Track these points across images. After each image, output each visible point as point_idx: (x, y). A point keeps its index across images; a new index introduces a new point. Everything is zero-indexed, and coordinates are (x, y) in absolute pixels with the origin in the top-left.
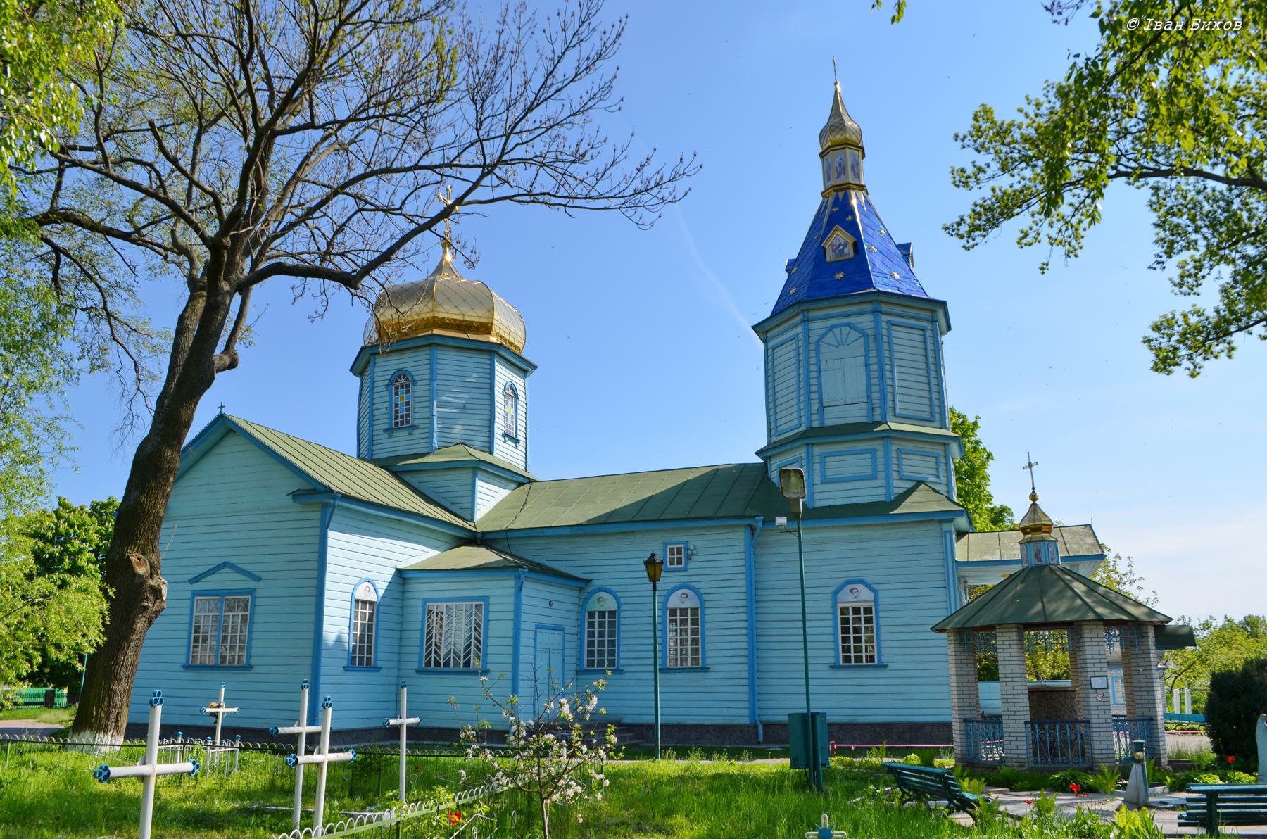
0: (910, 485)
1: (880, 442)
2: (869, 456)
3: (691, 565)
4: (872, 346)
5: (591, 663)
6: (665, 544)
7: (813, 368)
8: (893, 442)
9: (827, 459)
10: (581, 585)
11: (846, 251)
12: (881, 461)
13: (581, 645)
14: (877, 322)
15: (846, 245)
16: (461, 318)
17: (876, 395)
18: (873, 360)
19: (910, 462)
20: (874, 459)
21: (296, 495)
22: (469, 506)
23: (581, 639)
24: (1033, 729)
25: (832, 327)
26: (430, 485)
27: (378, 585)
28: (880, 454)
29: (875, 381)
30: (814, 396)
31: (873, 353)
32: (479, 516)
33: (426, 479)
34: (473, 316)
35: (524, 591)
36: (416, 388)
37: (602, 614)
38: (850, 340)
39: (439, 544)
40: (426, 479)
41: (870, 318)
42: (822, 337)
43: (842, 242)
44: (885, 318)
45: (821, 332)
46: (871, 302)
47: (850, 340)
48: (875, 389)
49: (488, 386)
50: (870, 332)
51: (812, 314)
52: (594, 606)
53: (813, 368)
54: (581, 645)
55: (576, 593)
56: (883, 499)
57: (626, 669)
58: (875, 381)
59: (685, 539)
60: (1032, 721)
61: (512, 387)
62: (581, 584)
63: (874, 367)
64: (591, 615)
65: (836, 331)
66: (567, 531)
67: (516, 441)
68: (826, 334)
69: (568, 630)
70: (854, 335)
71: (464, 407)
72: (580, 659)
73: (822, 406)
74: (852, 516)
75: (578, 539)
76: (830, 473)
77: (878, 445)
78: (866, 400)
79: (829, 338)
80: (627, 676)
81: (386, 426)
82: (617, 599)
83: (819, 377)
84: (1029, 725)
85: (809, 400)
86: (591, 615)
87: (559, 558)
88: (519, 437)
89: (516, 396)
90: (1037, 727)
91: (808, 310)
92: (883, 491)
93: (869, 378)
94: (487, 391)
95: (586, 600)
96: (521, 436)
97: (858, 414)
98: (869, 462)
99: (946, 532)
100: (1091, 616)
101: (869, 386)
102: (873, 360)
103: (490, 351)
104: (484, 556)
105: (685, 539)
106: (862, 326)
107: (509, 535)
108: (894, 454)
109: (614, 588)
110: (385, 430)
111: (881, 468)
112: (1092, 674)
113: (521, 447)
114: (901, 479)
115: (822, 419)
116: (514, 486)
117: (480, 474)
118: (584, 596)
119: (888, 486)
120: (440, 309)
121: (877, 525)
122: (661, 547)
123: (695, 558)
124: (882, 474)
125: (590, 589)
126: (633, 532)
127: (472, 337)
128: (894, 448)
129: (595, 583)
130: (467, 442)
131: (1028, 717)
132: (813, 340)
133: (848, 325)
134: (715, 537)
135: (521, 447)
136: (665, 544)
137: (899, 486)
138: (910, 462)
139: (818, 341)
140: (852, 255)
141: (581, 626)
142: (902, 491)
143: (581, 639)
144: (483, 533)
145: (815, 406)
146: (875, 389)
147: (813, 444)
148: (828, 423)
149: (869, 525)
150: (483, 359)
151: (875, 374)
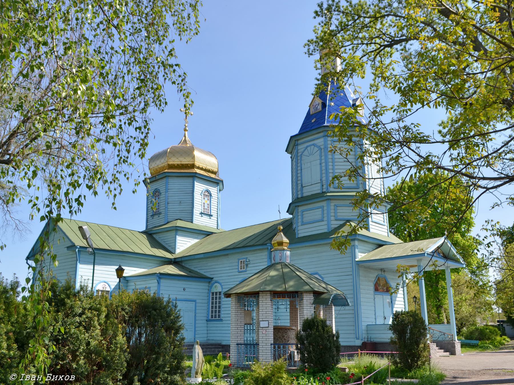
0: (342, 222)
1: (325, 202)
2: (321, 209)
3: (248, 269)
4: (323, 154)
5: (212, 317)
6: (239, 259)
7: (299, 168)
8: (332, 201)
9: (304, 213)
10: (209, 280)
11: (319, 107)
12: (325, 212)
13: (208, 308)
14: (325, 142)
15: (318, 105)
16: (179, 163)
17: (324, 179)
18: (323, 161)
19: (341, 211)
20: (323, 211)
21: (68, 248)
22: (174, 247)
23: (209, 305)
24: (274, 347)
25: (307, 147)
26: (162, 238)
27: (110, 283)
28: (325, 208)
29: (324, 171)
30: (299, 182)
31: (323, 158)
32: (178, 251)
33: (161, 236)
34: (185, 161)
35: (161, 284)
36: (162, 196)
37: (216, 293)
38: (314, 152)
39: (151, 264)
40: (161, 236)
41: (322, 140)
42: (303, 152)
43: (317, 103)
44: (329, 139)
45: (302, 150)
46: (323, 132)
47: (314, 152)
48: (324, 175)
49: (191, 192)
50: (322, 147)
51: (299, 142)
52: (214, 290)
53: (299, 168)
54: (208, 308)
55: (207, 284)
56: (326, 231)
57: (224, 319)
58: (324, 171)
59: (246, 256)
60: (274, 344)
61: (207, 191)
62: (209, 280)
63: (323, 164)
64: (213, 293)
65: (309, 148)
66: (202, 256)
67: (210, 216)
68: (304, 150)
69: (198, 301)
70: (316, 149)
71: (180, 203)
72: (208, 315)
73: (302, 187)
74: (309, 241)
75: (209, 259)
76: (305, 220)
77: (324, 204)
78: (319, 181)
79: (306, 153)
80: (224, 322)
81: (151, 214)
82: (222, 286)
83: (301, 172)
84: (273, 346)
85: (297, 184)
86: (213, 293)
87: (203, 268)
88: (212, 214)
89: (211, 195)
90: (277, 347)
91: (298, 140)
92: (326, 227)
93: (321, 170)
94: (191, 194)
95: (211, 287)
96: (214, 212)
97: (316, 189)
98: (320, 213)
99: (352, 246)
100: (307, 288)
101: (321, 174)
102: (323, 161)
103: (193, 176)
104: (171, 269)
105: (246, 256)
106: (319, 144)
107: (183, 259)
108: (332, 207)
109: (221, 281)
110: (151, 216)
111: (325, 215)
112: (261, 320)
113: (214, 218)
114: (336, 220)
115: (302, 193)
116: (204, 236)
117: (179, 232)
118: (210, 285)
119: (328, 224)
120: (170, 160)
121: (318, 245)
122: (237, 261)
123: (249, 266)
124: (325, 219)
125: (213, 282)
126: (227, 255)
127: (182, 171)
128: (333, 204)
129: (215, 279)
130: (181, 218)
131: (272, 342)
132: (299, 154)
133: (313, 145)
134: (258, 255)
135: (214, 218)
136: (239, 259)
137: (335, 224)
138: (341, 211)
139: (301, 155)
140: (321, 109)
141: (209, 299)
142: (336, 226)
143: (209, 305)
144: (175, 259)
145: (299, 187)
146: (324, 175)
147: (298, 206)
148: (305, 195)
149: (320, 245)
150: (190, 180)
151: (324, 168)
